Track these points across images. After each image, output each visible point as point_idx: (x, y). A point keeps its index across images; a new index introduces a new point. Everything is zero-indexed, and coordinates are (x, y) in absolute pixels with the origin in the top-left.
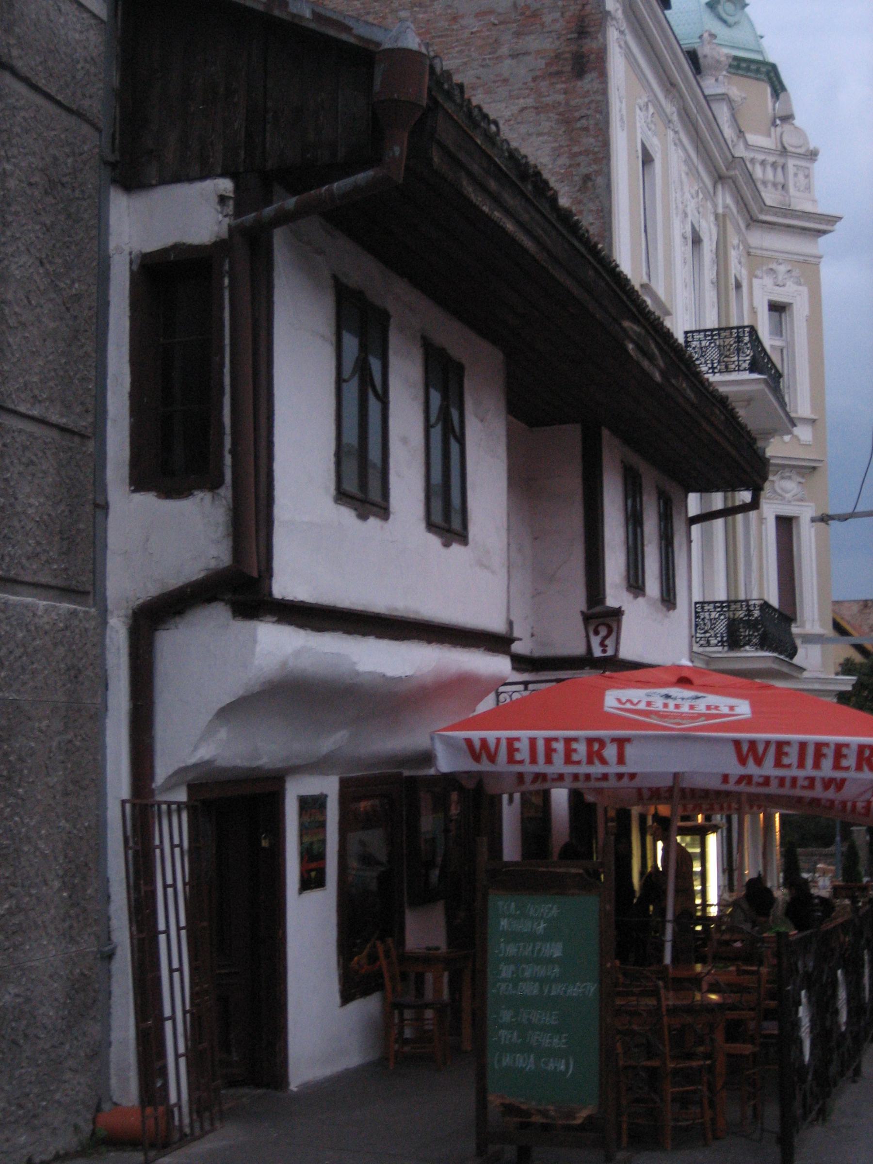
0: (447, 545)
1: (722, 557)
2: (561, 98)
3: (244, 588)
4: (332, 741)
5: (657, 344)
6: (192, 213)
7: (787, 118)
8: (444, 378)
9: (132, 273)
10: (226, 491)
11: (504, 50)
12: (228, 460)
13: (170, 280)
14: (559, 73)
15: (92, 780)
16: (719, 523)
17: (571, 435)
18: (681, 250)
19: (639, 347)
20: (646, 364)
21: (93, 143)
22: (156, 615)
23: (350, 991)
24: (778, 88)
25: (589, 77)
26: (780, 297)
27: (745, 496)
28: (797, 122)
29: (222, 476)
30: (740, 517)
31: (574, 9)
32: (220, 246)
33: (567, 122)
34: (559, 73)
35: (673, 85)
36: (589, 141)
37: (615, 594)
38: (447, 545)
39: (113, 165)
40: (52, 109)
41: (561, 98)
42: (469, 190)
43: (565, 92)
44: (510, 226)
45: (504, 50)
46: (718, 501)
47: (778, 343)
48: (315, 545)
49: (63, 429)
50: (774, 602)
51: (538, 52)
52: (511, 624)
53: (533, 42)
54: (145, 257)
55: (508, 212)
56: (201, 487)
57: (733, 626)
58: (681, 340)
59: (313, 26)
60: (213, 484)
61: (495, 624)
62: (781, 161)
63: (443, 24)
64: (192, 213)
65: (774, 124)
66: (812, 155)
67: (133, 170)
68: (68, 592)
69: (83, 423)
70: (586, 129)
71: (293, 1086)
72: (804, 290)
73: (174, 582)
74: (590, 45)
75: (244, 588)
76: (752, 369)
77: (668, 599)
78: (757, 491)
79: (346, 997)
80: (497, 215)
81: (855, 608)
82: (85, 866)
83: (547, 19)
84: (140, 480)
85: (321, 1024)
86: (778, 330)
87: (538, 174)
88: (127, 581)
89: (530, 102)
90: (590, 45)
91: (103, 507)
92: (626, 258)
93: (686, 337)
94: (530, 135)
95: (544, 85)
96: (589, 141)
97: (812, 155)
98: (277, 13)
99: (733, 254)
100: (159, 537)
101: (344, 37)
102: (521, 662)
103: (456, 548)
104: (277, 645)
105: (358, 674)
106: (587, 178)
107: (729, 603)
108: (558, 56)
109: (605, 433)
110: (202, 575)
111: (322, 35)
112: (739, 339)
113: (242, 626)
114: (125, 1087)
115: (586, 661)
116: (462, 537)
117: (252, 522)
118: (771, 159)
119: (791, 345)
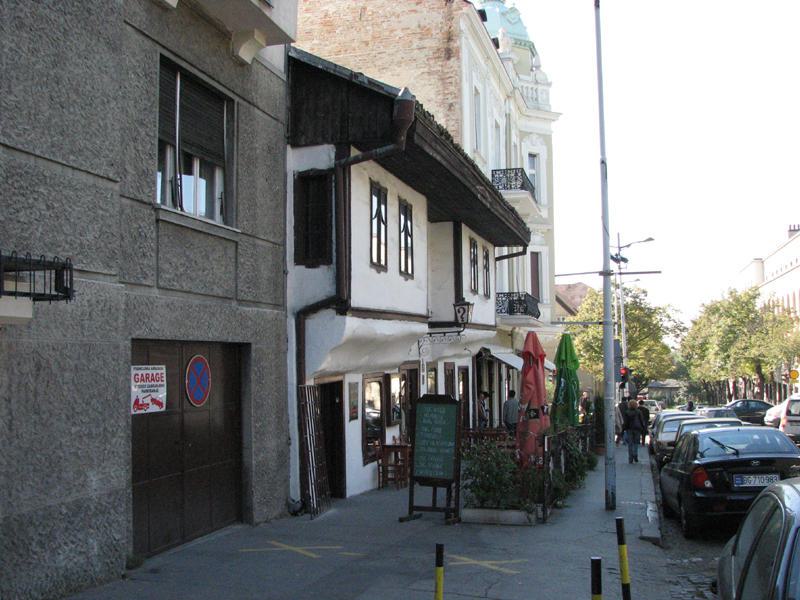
0: (379, 272)
1: (508, 274)
2: (440, 68)
3: (340, 303)
4: (364, 360)
5: (489, 193)
6: (321, 157)
7: (538, 67)
8: (406, 209)
9: (295, 180)
10: (334, 266)
11: (414, 46)
12: (334, 254)
13: (309, 182)
14: (439, 57)
15: (282, 377)
16: (506, 261)
17: (449, 227)
18: (491, 131)
19: (482, 195)
20: (484, 201)
21: (282, 130)
22: (303, 315)
23: (367, 460)
24: (533, 53)
25: (452, 59)
26: (534, 151)
27: (521, 249)
28: (542, 68)
29: (332, 260)
30: (515, 259)
31: (446, 28)
32: (331, 171)
33: (442, 79)
34: (439, 57)
35: (488, 58)
36: (452, 88)
37: (467, 296)
38: (379, 272)
39: (288, 138)
40: (269, 118)
41: (440, 68)
42: (427, 149)
43: (442, 66)
44: (438, 158)
45: (414, 46)
46: (505, 251)
47: (533, 172)
48: (365, 288)
49: (273, 243)
50: (530, 293)
51: (430, 47)
52: (428, 310)
53: (427, 43)
54: (300, 173)
55: (439, 153)
56: (324, 264)
57: (511, 304)
58: (489, 177)
59: (369, 87)
60: (328, 262)
61: (423, 312)
62: (535, 87)
63: (387, 33)
64: (321, 157)
65: (532, 70)
66: (549, 84)
67: (296, 139)
68: (276, 306)
69: (280, 241)
70: (451, 83)
71: (348, 495)
72: (545, 148)
73: (312, 302)
74: (454, 45)
75: (340, 303)
76: (523, 187)
77: (487, 296)
78: (525, 246)
79: (365, 464)
80: (435, 155)
81: (564, 289)
82: (282, 409)
83: (434, 32)
84: (298, 262)
85: (359, 475)
86: (533, 166)
87: (447, 132)
88: (294, 299)
89: (426, 70)
90: (454, 45)
91: (285, 273)
92: (468, 150)
93: (493, 176)
94: (425, 85)
95: (432, 62)
96: (452, 88)
97: (549, 84)
98: (354, 80)
99: (513, 132)
100: (306, 283)
101: (381, 91)
102: (432, 325)
103: (410, 281)
104: (352, 325)
105: (376, 334)
106: (451, 105)
107: (509, 294)
108: (439, 50)
109: (463, 225)
110: (324, 298)
111: (371, 90)
112: (516, 174)
113: (339, 318)
114: (295, 493)
115: (455, 324)
116: (412, 276)
117: (343, 278)
118: (530, 86)
119: (538, 172)
